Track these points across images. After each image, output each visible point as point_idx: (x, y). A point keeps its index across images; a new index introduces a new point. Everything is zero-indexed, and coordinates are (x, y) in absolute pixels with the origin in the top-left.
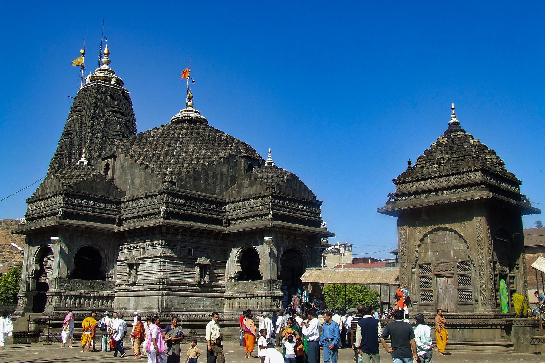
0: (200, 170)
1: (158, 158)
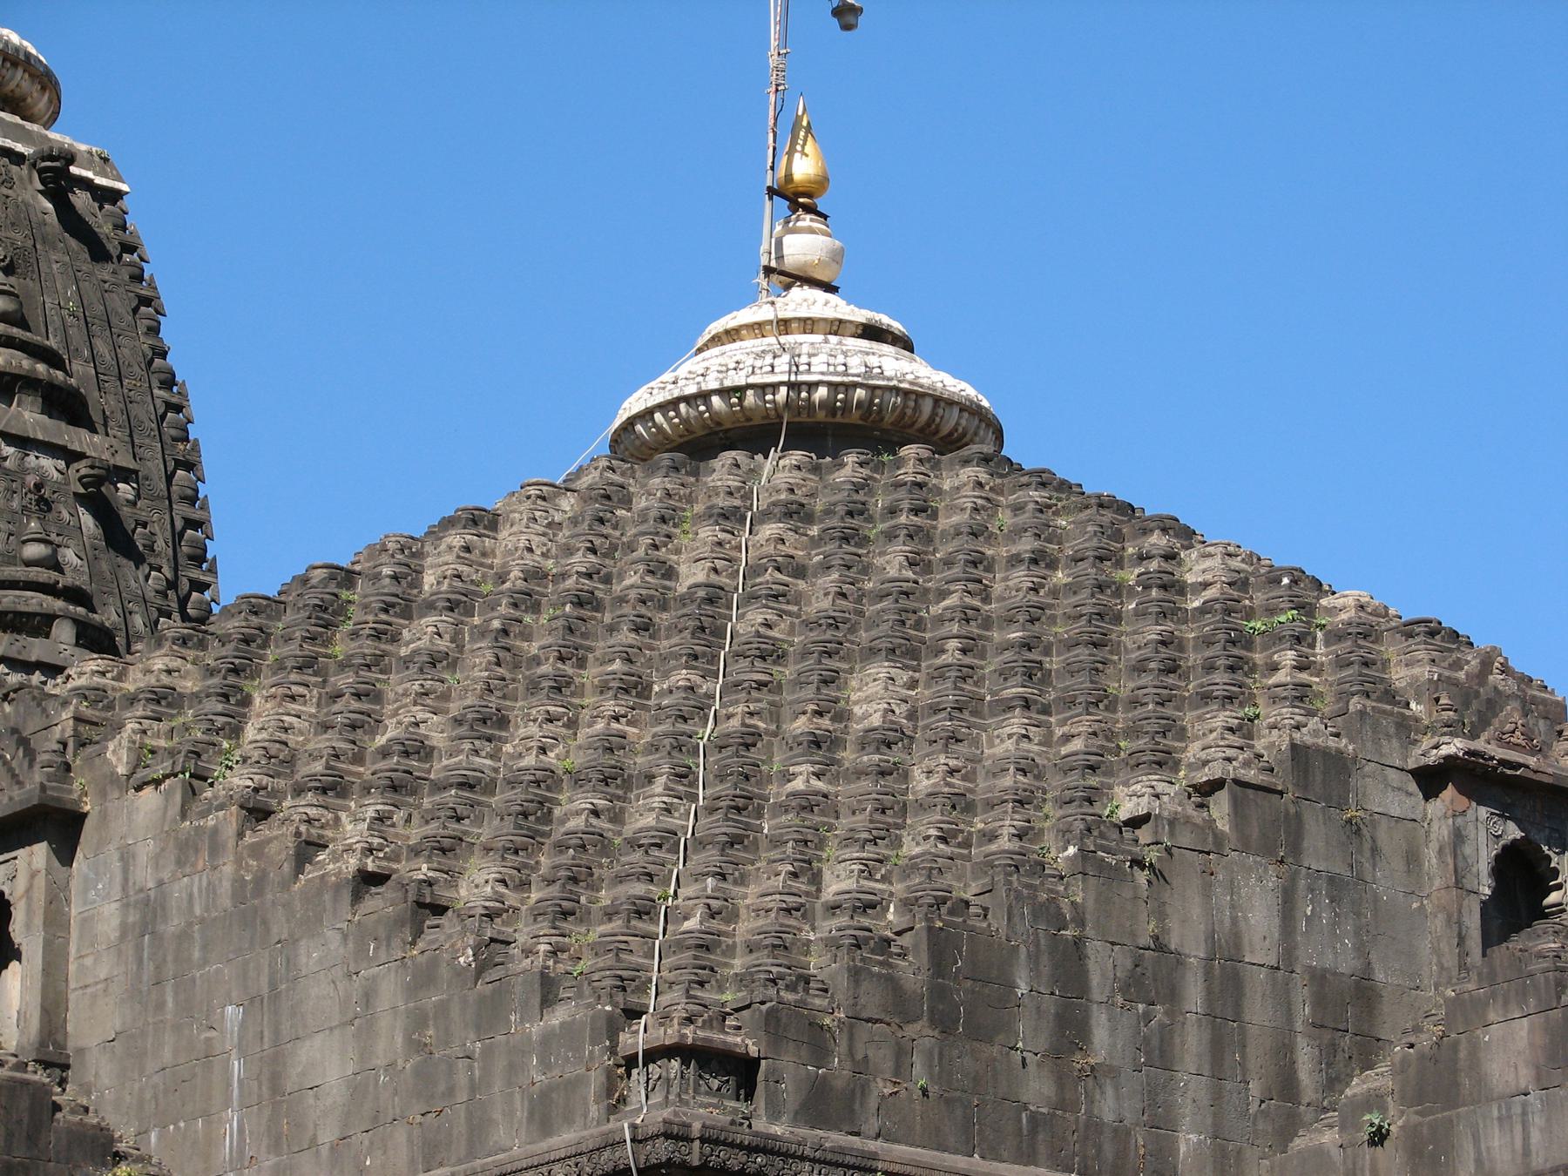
0: (998, 922)
1: (535, 815)
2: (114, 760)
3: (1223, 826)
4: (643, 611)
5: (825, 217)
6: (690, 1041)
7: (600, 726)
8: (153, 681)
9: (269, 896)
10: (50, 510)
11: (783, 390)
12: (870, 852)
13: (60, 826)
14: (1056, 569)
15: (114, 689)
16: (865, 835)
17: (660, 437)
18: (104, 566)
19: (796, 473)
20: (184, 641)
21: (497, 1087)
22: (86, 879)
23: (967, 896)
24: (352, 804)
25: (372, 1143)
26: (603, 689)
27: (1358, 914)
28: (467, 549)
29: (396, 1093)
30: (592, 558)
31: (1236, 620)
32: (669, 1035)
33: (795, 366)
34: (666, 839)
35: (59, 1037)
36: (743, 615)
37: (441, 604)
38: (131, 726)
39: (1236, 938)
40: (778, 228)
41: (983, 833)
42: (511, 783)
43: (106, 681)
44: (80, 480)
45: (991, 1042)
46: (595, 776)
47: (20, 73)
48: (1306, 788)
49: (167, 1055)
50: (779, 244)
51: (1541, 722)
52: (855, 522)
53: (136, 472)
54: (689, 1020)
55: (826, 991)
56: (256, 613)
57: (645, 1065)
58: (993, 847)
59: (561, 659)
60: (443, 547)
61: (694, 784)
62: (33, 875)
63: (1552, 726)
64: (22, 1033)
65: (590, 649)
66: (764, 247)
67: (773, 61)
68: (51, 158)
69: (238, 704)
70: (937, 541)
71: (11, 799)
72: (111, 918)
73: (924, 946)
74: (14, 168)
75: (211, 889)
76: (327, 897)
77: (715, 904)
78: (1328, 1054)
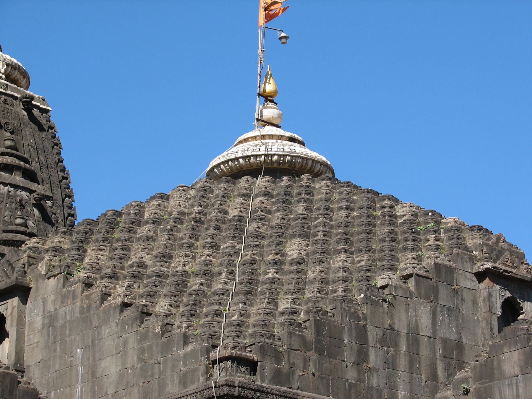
0: (338, 318)
1: (181, 284)
2: (41, 269)
3: (412, 289)
4: (217, 224)
5: (276, 104)
6: (234, 355)
7: (203, 258)
8: (55, 245)
9: (92, 312)
10: (24, 208)
11: (263, 157)
12: (294, 296)
13: (22, 291)
14: (354, 211)
15: (41, 248)
16: (293, 291)
17: (222, 173)
18: (42, 227)
19: (267, 183)
20: (65, 233)
21: (169, 372)
22: (31, 309)
23: (327, 310)
24: (120, 282)
25: (126, 393)
26: (204, 247)
27: (457, 320)
28: (159, 205)
29: (134, 376)
30: (201, 208)
31: (414, 226)
32: (227, 353)
33: (267, 149)
34: (225, 292)
35: (21, 362)
36: (250, 225)
37: (150, 222)
38: (46, 258)
39: (417, 327)
40: (261, 107)
41: (332, 291)
42: (173, 275)
43: (39, 245)
44: (34, 199)
45: (336, 359)
46: (202, 273)
47: (16, 72)
48: (439, 277)
49: (57, 367)
50: (261, 112)
51: (516, 259)
52: (287, 197)
53: (52, 197)
54: (234, 348)
55: (280, 339)
56: (89, 225)
57: (219, 363)
58: (336, 294)
59: (190, 238)
60: (151, 205)
61: (235, 276)
62: (13, 308)
63: (520, 261)
64: (9, 360)
65: (200, 235)
66: (257, 112)
67: (260, 53)
68: (26, 98)
69: (83, 252)
70: (314, 203)
71: (6, 283)
72: (39, 321)
73: (313, 326)
74: (14, 101)
75: (73, 310)
76: (111, 311)
77: (242, 312)
78: (448, 366)
